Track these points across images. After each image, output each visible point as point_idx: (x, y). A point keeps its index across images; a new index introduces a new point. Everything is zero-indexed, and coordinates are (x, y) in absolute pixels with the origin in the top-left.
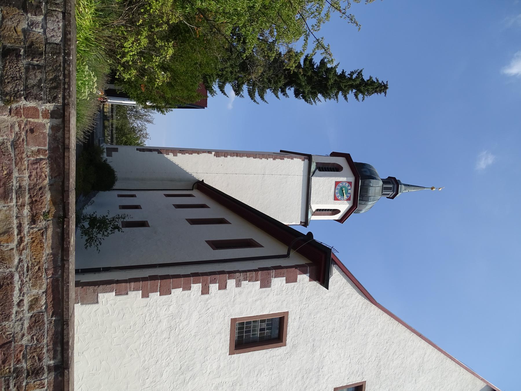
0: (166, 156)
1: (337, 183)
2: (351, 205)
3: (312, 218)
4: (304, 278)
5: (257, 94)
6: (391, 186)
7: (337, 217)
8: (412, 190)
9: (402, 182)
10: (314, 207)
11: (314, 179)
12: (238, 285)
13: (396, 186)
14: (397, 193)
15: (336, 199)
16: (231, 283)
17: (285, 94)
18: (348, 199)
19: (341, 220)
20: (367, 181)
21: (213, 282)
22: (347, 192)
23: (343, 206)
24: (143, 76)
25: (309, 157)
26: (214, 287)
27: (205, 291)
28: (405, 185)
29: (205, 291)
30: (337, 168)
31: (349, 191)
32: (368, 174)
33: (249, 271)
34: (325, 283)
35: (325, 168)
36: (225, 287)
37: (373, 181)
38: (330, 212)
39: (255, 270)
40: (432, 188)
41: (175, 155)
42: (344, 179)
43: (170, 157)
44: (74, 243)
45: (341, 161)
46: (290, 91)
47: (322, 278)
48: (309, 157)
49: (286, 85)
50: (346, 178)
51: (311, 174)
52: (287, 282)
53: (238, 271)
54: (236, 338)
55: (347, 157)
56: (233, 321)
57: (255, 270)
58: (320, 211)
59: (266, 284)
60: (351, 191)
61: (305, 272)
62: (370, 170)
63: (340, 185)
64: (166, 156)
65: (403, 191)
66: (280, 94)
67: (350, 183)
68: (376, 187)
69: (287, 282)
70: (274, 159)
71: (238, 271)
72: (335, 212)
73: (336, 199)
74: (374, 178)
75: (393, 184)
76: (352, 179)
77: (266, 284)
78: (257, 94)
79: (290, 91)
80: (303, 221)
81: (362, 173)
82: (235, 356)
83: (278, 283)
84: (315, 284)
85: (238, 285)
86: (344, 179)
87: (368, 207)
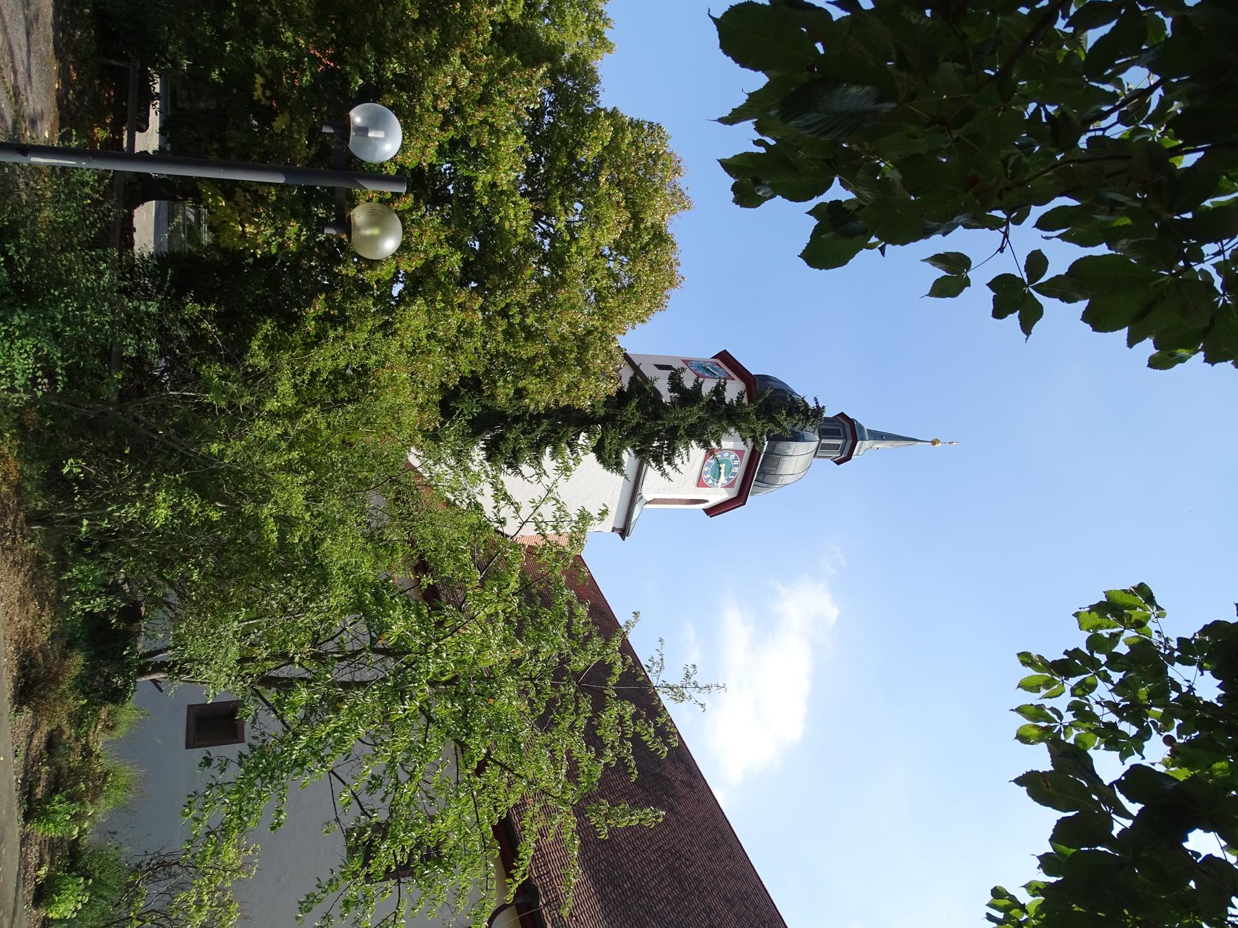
6: (840, 442)
13: (850, 442)
14: (848, 458)
19: (712, 511)
20: (782, 446)
22: (728, 472)
28: (878, 436)
31: (736, 470)
37: (794, 444)
40: (934, 443)
67: (740, 453)
73: (701, 483)
80: (620, 526)
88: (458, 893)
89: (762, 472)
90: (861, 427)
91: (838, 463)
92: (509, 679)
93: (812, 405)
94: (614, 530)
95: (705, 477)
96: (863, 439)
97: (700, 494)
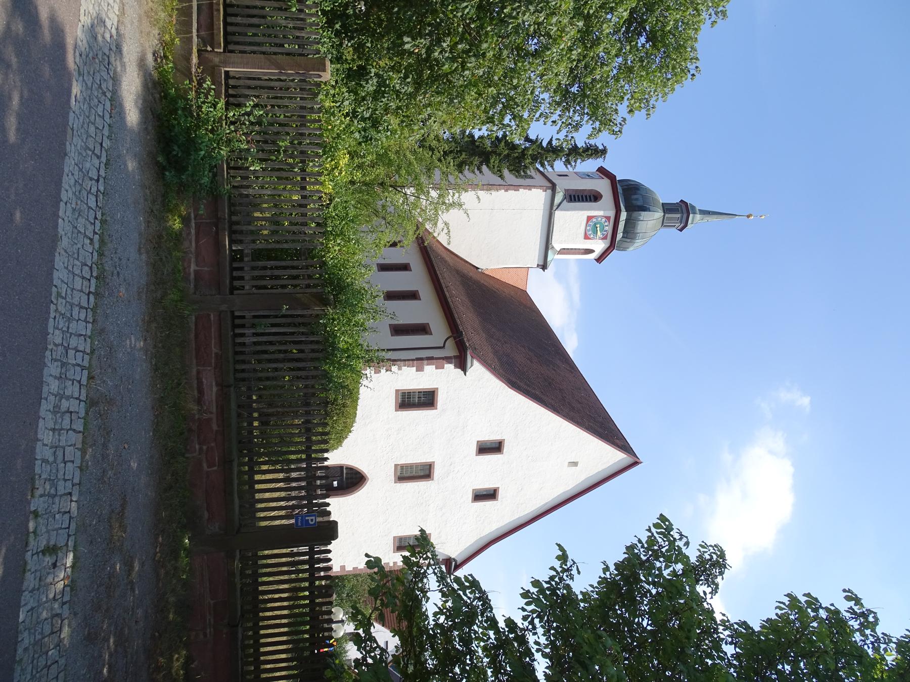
1: (589, 218)
2: (608, 245)
6: (679, 216)
8: (714, 219)
10: (557, 244)
11: (558, 215)
13: (685, 216)
14: (686, 225)
15: (586, 237)
16: (395, 368)
18: (605, 238)
19: (599, 259)
20: (635, 214)
22: (602, 230)
23: (599, 246)
28: (704, 213)
30: (594, 197)
31: (606, 228)
32: (639, 203)
33: (408, 360)
34: (464, 369)
37: (643, 213)
39: (413, 360)
40: (748, 216)
42: (601, 213)
44: (144, 120)
50: (602, 211)
52: (437, 368)
53: (400, 360)
54: (400, 400)
56: (397, 391)
57: (413, 360)
58: (564, 251)
59: (420, 369)
60: (609, 228)
61: (451, 363)
62: (645, 198)
63: (594, 220)
65: (696, 219)
67: (608, 218)
69: (437, 368)
70: (506, 191)
71: (400, 360)
73: (586, 237)
76: (612, 213)
77: (420, 369)
80: (541, 263)
82: (399, 413)
83: (430, 369)
85: (400, 369)
86: (601, 213)
87: (636, 245)
88: (178, 660)
89: (625, 232)
90: (693, 207)
91: (681, 230)
92: (178, 349)
93: (601, 147)
94: (538, 265)
95: (588, 233)
96: (694, 213)
97: (588, 245)
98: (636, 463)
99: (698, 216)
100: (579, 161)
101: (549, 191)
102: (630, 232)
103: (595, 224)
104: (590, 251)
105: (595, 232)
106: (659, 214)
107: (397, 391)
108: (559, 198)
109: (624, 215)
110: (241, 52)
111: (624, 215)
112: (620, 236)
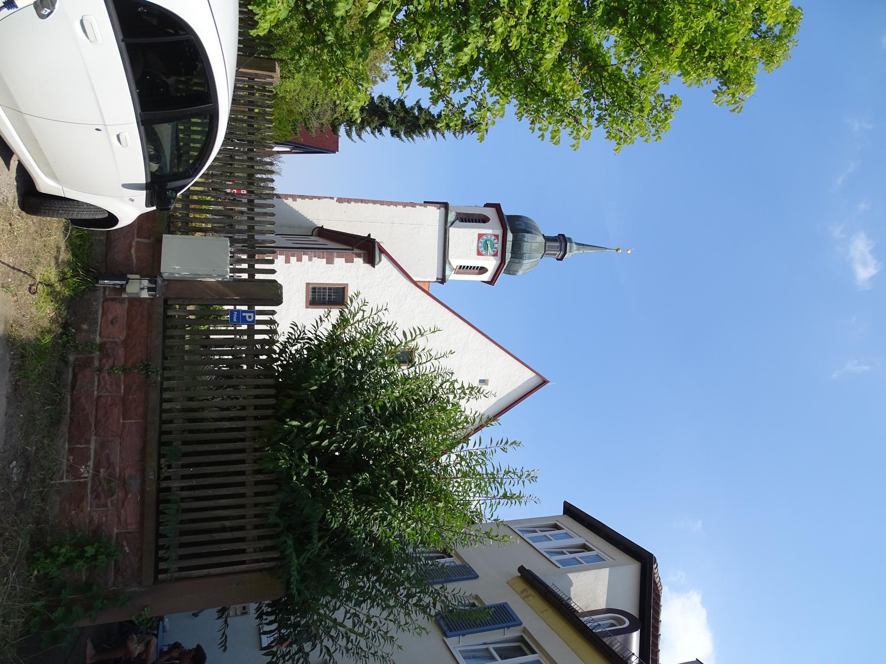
0: (285, 201)
2: (499, 262)
3: (452, 276)
4: (359, 261)
5: (354, 134)
6: (558, 244)
7: (487, 277)
9: (574, 240)
10: (455, 261)
11: (452, 231)
12: (310, 260)
13: (563, 244)
15: (479, 254)
16: (305, 258)
17: (381, 133)
18: (495, 255)
19: (492, 282)
21: (293, 255)
22: (492, 247)
23: (491, 263)
24: (319, 114)
25: (445, 205)
26: (293, 259)
27: (287, 261)
28: (577, 244)
29: (287, 261)
31: (496, 246)
32: (523, 227)
35: (466, 218)
36: (301, 260)
37: (527, 235)
38: (477, 271)
40: (617, 250)
41: (294, 200)
42: (490, 231)
43: (289, 202)
45: (491, 213)
46: (386, 131)
47: (371, 260)
48: (445, 205)
49: (381, 125)
50: (491, 230)
51: (449, 224)
55: (497, 207)
58: (463, 269)
59: (330, 261)
60: (499, 246)
62: (526, 224)
64: (285, 201)
65: (573, 253)
66: (377, 134)
67: (497, 236)
68: (533, 243)
72: (483, 270)
73: (479, 254)
74: (528, 232)
75: (560, 241)
76: (499, 232)
77: (330, 261)
78: (354, 134)
79: (386, 131)
81: (515, 227)
82: (310, 310)
83: (339, 262)
84: (368, 266)
86: (490, 231)
89: (513, 252)
91: (561, 259)
98: (545, 382)
99: (575, 246)
100: (466, 132)
101: (443, 209)
102: (518, 253)
103: (486, 241)
104: (483, 270)
105: (486, 248)
106: (540, 239)
107: (308, 284)
108: (452, 217)
109: (510, 236)
110: (143, 452)
111: (510, 236)
112: (508, 255)
